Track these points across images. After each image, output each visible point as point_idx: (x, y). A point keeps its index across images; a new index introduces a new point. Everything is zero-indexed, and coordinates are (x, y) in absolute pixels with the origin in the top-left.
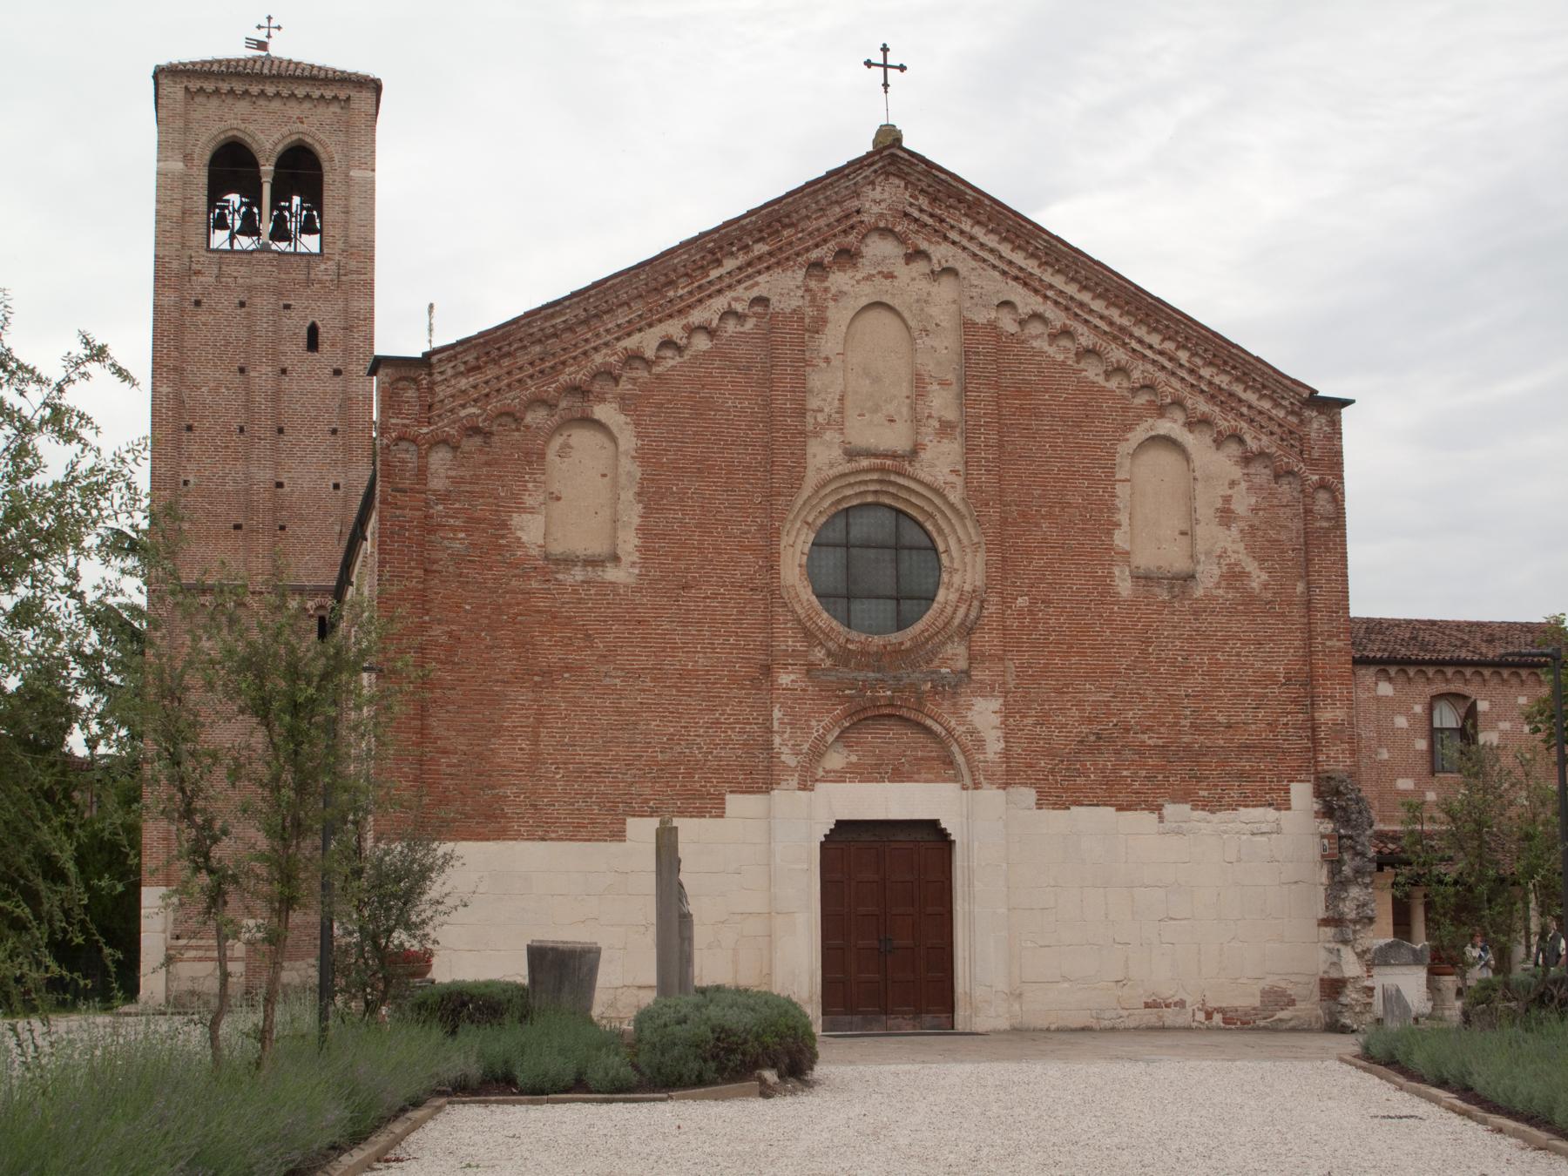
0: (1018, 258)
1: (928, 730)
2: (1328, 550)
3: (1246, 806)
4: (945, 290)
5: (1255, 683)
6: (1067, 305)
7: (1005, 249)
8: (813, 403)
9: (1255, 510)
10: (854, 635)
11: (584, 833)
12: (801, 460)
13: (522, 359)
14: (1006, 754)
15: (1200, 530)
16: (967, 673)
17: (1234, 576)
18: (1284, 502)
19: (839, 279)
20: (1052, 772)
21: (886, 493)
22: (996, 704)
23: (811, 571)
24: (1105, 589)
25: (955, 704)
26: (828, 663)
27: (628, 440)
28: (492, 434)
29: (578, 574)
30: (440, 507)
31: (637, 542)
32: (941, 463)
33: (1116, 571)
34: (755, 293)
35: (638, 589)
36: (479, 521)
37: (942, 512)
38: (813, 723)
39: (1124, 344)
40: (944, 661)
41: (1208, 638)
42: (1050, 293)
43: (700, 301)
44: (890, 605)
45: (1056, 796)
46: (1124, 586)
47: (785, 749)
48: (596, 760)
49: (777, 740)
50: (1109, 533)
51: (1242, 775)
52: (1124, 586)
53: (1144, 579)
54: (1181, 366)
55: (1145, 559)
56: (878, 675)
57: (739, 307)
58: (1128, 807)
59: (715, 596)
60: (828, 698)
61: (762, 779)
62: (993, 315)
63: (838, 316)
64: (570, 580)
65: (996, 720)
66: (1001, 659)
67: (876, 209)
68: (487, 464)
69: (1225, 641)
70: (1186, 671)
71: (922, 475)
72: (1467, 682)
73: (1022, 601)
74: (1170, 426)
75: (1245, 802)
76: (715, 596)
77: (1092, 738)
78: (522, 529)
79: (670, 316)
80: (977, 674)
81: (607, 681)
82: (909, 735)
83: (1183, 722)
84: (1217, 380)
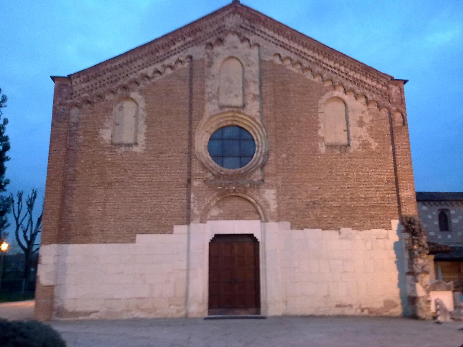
0: (281, 38)
1: (249, 201)
2: (401, 134)
3: (374, 228)
4: (255, 51)
5: (376, 183)
6: (298, 53)
7: (276, 36)
8: (208, 90)
9: (372, 121)
10: (224, 169)
11: (120, 240)
12: (203, 110)
13: (105, 77)
14: (278, 210)
15: (351, 129)
16: (263, 180)
17: (365, 145)
18: (383, 118)
19: (218, 49)
20: (296, 216)
21: (235, 120)
22: (273, 191)
23: (210, 149)
24: (316, 151)
25: (258, 192)
26: (212, 178)
27: (142, 104)
28: (94, 103)
29: (123, 149)
30: (75, 128)
31: (144, 138)
32: (253, 108)
33: (319, 144)
34: (187, 54)
35: (144, 154)
36: (88, 132)
37: (255, 126)
38: (206, 199)
39: (321, 66)
40: (255, 177)
41: (356, 167)
42: (293, 50)
43: (168, 57)
44: (238, 159)
45: (299, 224)
46: (323, 149)
47: (195, 209)
48: (127, 214)
49: (192, 205)
50: (316, 131)
51: (372, 217)
52: (323, 149)
53: (331, 147)
54: (342, 72)
55: (330, 139)
56: (230, 182)
57: (181, 59)
58: (327, 229)
59: (172, 156)
60: (211, 190)
61: (187, 220)
62: (272, 58)
63: (218, 62)
64: (120, 151)
65: (274, 197)
66: (275, 175)
67: (230, 25)
68: (92, 113)
69: (362, 167)
70: (347, 178)
71: (247, 113)
72: (448, 206)
73: (284, 155)
74: (339, 93)
75: (373, 226)
76: (172, 156)
77: (312, 203)
78: (103, 134)
79: (158, 62)
80: (266, 181)
81: (132, 186)
82: (242, 203)
83: (347, 197)
84: (355, 76)
